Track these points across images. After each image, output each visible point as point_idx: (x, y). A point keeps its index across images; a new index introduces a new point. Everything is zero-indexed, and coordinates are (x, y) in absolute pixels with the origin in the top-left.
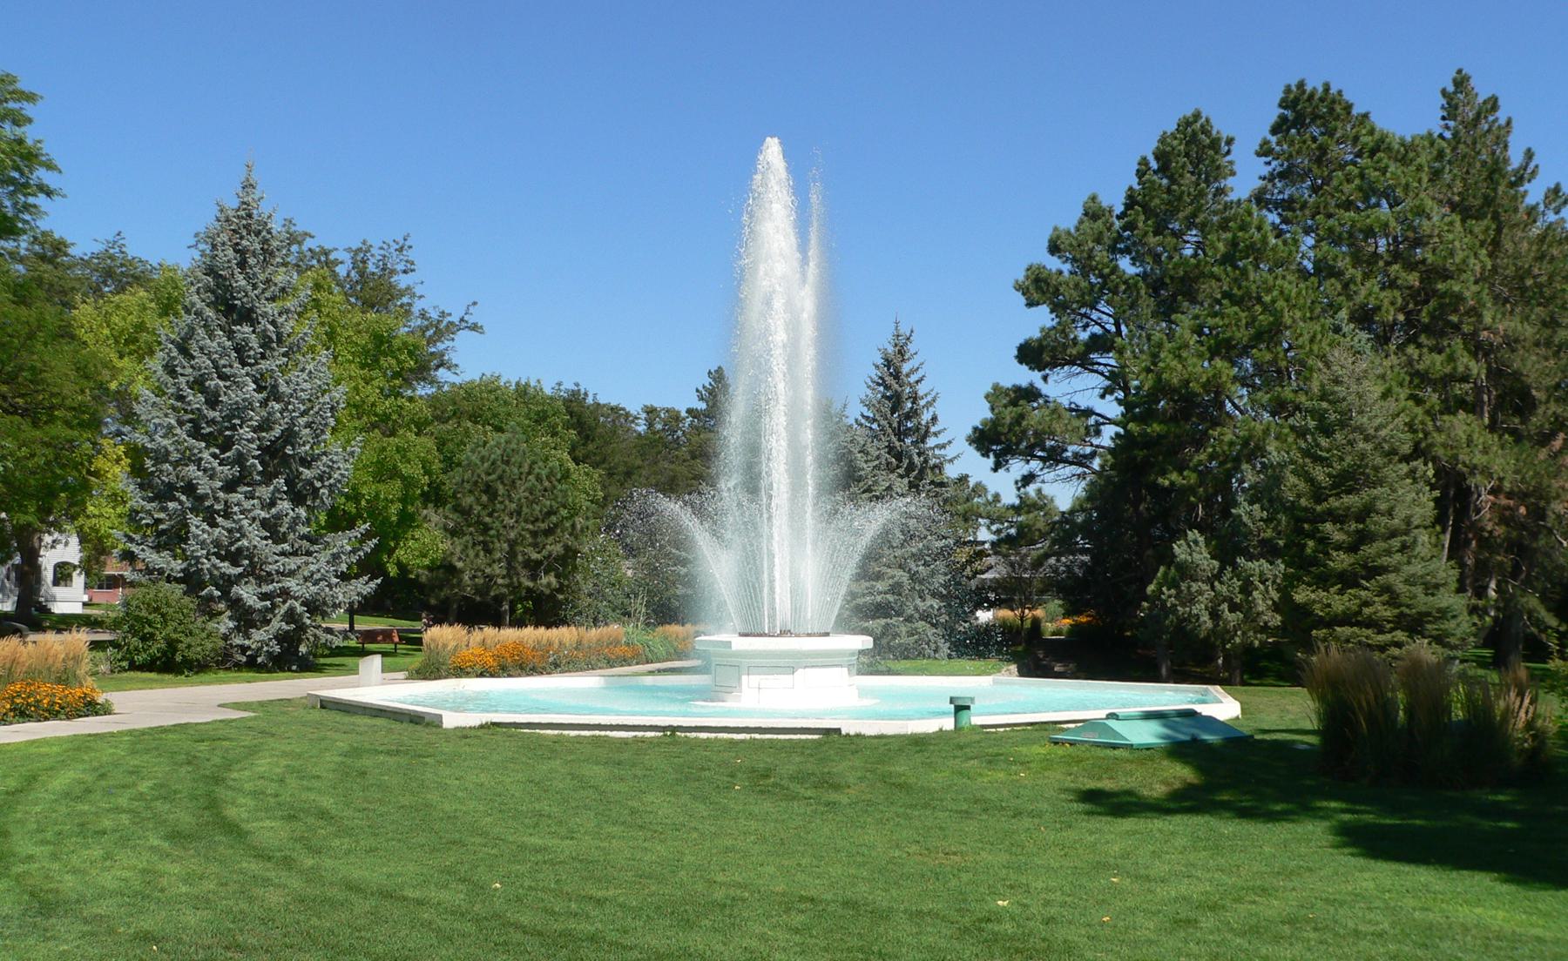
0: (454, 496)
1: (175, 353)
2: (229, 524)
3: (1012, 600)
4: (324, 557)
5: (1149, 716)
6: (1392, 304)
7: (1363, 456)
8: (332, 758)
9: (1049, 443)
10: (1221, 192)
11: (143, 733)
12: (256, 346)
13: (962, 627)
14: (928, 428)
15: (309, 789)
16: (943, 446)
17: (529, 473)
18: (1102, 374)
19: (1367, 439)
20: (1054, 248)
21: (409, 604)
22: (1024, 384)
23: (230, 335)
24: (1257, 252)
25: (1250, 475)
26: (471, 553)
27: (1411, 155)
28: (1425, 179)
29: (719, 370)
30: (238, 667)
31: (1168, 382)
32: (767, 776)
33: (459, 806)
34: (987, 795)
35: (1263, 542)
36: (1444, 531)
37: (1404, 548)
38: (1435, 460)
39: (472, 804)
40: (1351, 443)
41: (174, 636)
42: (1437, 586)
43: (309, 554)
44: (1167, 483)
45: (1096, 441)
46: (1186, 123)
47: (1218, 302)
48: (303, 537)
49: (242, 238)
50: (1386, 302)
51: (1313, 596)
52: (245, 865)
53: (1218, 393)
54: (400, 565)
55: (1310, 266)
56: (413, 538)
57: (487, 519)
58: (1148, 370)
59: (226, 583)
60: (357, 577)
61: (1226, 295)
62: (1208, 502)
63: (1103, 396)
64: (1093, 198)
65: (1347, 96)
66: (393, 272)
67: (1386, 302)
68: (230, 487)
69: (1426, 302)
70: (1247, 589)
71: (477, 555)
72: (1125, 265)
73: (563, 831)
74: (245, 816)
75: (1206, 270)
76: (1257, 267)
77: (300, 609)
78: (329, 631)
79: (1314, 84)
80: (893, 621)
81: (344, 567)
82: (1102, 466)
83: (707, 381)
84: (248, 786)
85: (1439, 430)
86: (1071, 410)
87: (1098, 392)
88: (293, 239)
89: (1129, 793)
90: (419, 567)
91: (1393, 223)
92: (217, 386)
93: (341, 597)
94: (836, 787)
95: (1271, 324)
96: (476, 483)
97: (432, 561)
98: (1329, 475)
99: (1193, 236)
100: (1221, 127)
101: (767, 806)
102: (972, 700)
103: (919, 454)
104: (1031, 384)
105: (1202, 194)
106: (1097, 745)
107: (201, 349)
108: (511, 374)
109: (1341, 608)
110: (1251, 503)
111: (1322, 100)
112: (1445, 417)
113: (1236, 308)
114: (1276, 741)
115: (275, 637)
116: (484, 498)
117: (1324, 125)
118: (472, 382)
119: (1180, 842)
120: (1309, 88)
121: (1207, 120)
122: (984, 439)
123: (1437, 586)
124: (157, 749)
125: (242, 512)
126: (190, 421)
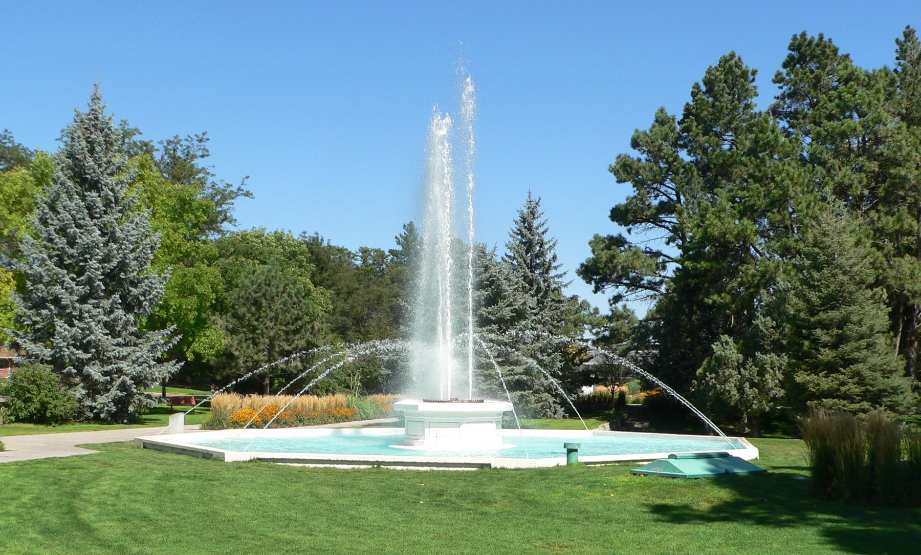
1: (47, 210)
2: (82, 325)
3: (606, 379)
5: (699, 456)
6: (860, 182)
7: (842, 285)
8: (151, 481)
9: (632, 275)
11: (25, 463)
15: (135, 501)
16: (560, 276)
17: (283, 292)
18: (667, 228)
19: (844, 273)
20: (635, 144)
21: (199, 377)
22: (615, 235)
23: (83, 198)
24: (771, 147)
25: (765, 297)
26: (244, 345)
27: (872, 83)
28: (882, 98)
30: (88, 420)
34: (589, 508)
35: (773, 342)
36: (896, 336)
37: (868, 346)
38: (889, 288)
39: (244, 512)
40: (834, 276)
41: (45, 399)
42: (891, 372)
43: (136, 345)
44: (711, 301)
45: (663, 274)
46: (725, 61)
48: (132, 334)
49: (91, 133)
50: (856, 182)
52: (93, 551)
53: (745, 242)
54: (194, 353)
56: (205, 335)
57: (255, 323)
59: (80, 365)
60: (167, 360)
62: (738, 314)
63: (668, 243)
64: (662, 110)
65: (835, 43)
66: (194, 156)
67: (856, 182)
68: (83, 300)
69: (884, 182)
70: (762, 372)
71: (248, 347)
72: (684, 155)
73: (305, 530)
74: (93, 518)
78: (149, 397)
79: (812, 34)
80: (526, 393)
81: (159, 354)
82: (667, 290)
83: (403, 231)
84: (95, 499)
85: (891, 267)
86: (646, 252)
87: (665, 240)
88: (127, 134)
90: (209, 355)
91: (860, 128)
92: (75, 232)
93: (157, 374)
94: (487, 503)
96: (247, 299)
97: (218, 352)
98: (819, 297)
100: (748, 64)
101: (441, 514)
102: (579, 445)
103: (544, 281)
104: (620, 235)
105: (735, 108)
106: (663, 476)
107: (64, 207)
109: (826, 386)
111: (817, 45)
112: (896, 259)
113: (757, 185)
114: (782, 474)
115: (113, 401)
116: (253, 309)
117: (818, 62)
119: (717, 540)
120: (809, 37)
121: (739, 59)
122: (588, 272)
123: (891, 372)
124: (34, 474)
125: (90, 317)
126: (57, 256)
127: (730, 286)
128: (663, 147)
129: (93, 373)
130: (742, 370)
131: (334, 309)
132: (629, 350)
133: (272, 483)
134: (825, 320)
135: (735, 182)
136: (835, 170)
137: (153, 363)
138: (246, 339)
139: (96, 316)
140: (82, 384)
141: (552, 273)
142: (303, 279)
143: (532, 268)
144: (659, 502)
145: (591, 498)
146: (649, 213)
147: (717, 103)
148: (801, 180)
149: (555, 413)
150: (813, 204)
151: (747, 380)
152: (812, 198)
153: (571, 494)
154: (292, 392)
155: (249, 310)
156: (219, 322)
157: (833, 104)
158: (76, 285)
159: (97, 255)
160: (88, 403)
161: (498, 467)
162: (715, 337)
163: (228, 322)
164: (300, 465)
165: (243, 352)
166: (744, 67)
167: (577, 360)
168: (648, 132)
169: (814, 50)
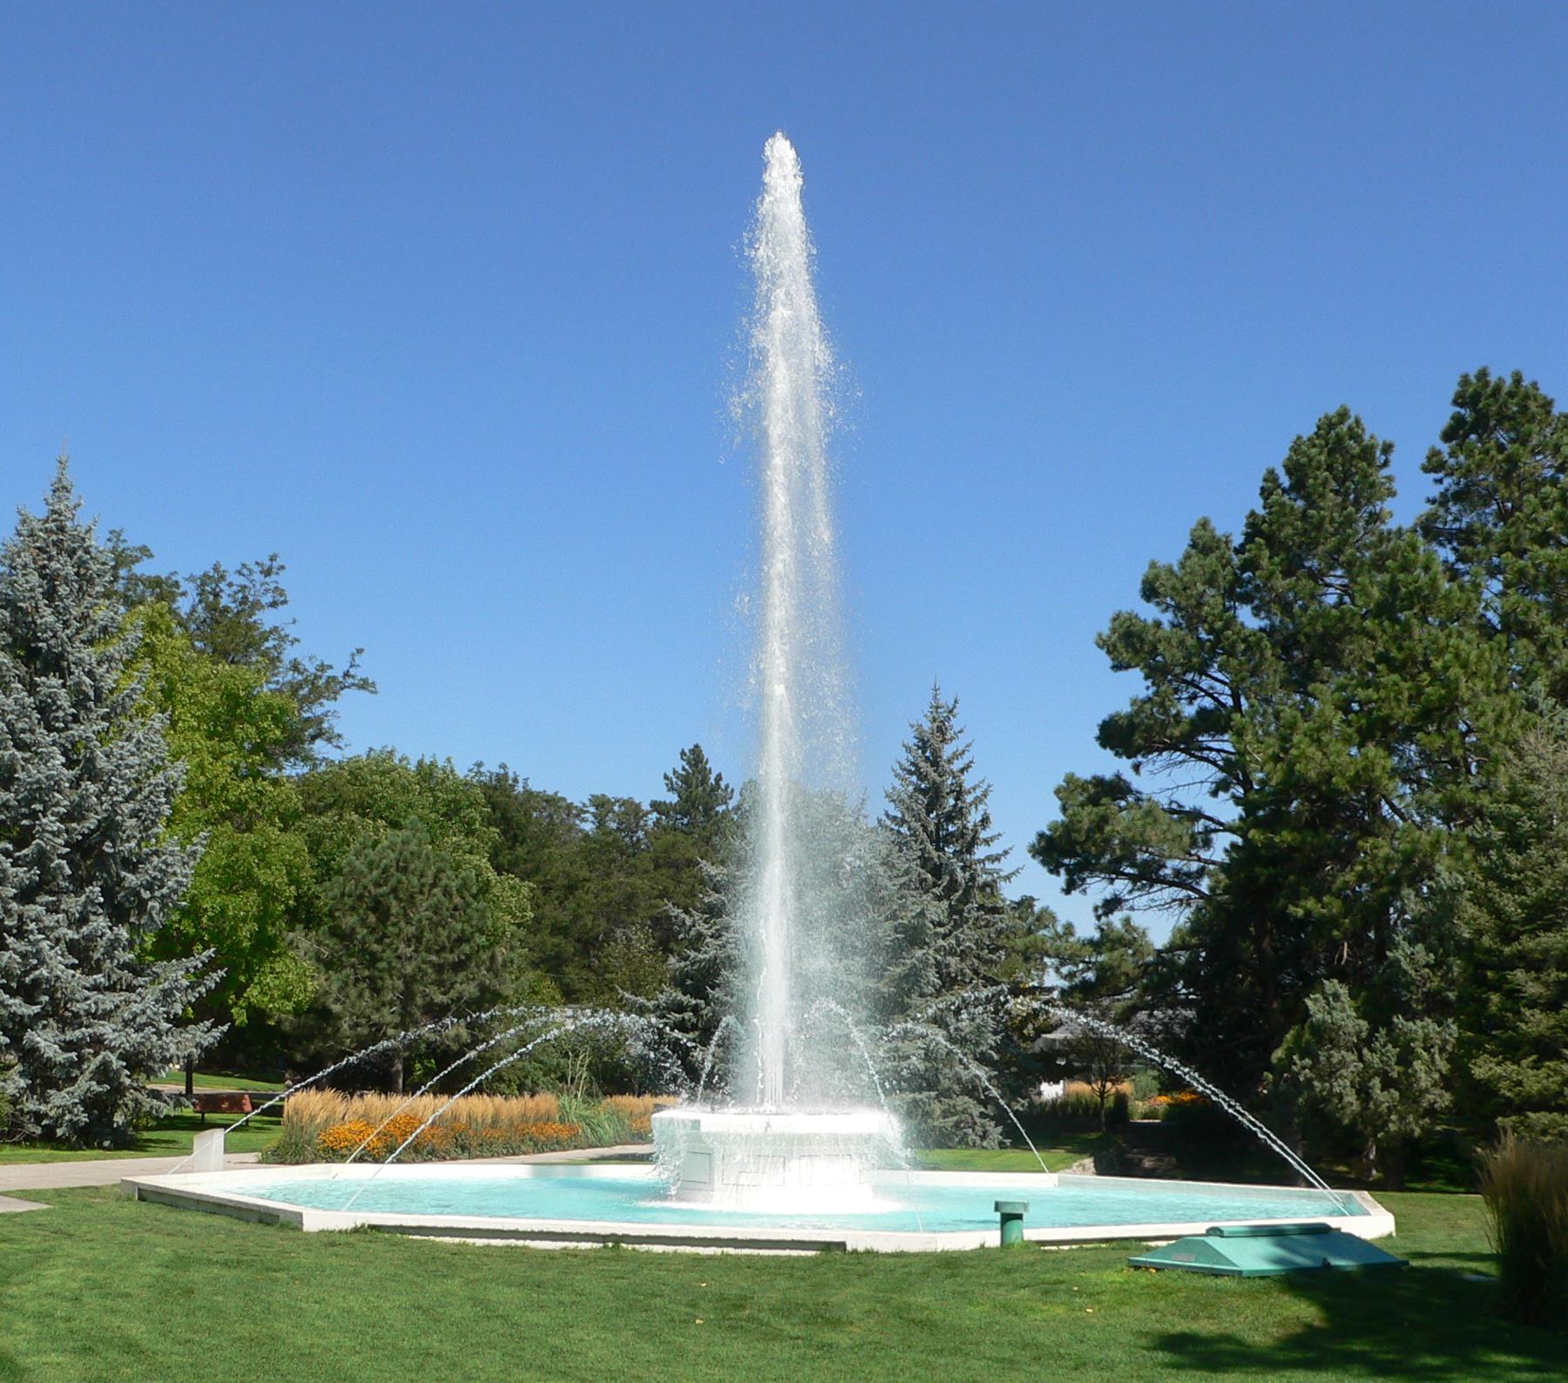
0: (331, 915)
2: (22, 946)
5: (1257, 1232)
8: (148, 1270)
9: (1141, 857)
10: (1375, 518)
12: (66, 705)
13: (1021, 1105)
15: (113, 1312)
16: (997, 858)
17: (434, 885)
18: (1214, 763)
20: (1150, 591)
21: (264, 1058)
22: (1108, 775)
23: (32, 689)
24: (1423, 600)
25: (1412, 903)
26: (353, 992)
29: (696, 750)
30: (31, 1141)
32: (742, 1307)
34: (1041, 1338)
39: (334, 1338)
40: (1551, 861)
43: (131, 988)
44: (1301, 912)
45: (1205, 855)
46: (1328, 426)
47: (1372, 668)
48: (122, 967)
49: (50, 559)
51: (1499, 1070)
53: (1370, 792)
57: (375, 947)
58: (1276, 759)
61: (1383, 658)
62: (1357, 939)
63: (1214, 794)
64: (1204, 524)
65: (1546, 390)
66: (257, 605)
70: (1406, 1058)
71: (360, 996)
72: (1247, 618)
74: (23, 1346)
75: (1355, 626)
77: (117, 1065)
78: (156, 1095)
79: (1501, 373)
81: (178, 1008)
82: (1212, 889)
83: (680, 765)
84: (31, 1306)
87: (1208, 787)
89: (1227, 1338)
90: (281, 1012)
92: (13, 756)
94: (835, 1324)
95: (1442, 698)
96: (360, 898)
98: (1522, 905)
99: (1337, 577)
100: (1375, 430)
101: (738, 1347)
102: (1025, 1206)
103: (964, 869)
104: (1118, 776)
105: (1349, 521)
108: (412, 749)
109: (1536, 1087)
110: (1412, 942)
111: (1511, 395)
113: (1395, 677)
115: (82, 1102)
116: (372, 918)
117: (1514, 429)
118: (357, 759)
120: (1493, 379)
121: (1357, 421)
122: (1054, 850)
125: (40, 931)
128: (1206, 599)
129: (43, 1044)
130: (1365, 1051)
131: (537, 920)
132: (1133, 1009)
133: (394, 1277)
134: (1532, 951)
135: (1348, 670)
136: (1555, 647)
138: (357, 980)
139: (52, 929)
140: (19, 1067)
141: (980, 852)
142: (475, 859)
143: (940, 841)
145: (1047, 1318)
146: (1176, 733)
147: (1312, 512)
149: (984, 1137)
150: (1508, 716)
151: (1377, 1074)
152: (1506, 704)
153: (1005, 1307)
154: (448, 1087)
155: (363, 921)
156: (303, 941)
157: (1551, 513)
158: (13, 865)
159: (57, 804)
160: (31, 1105)
161: (861, 1249)
162: (1311, 984)
163: (319, 943)
164: (457, 1240)
165: (352, 1010)
166: (1366, 437)
167: (1029, 1030)
168: (1176, 568)
169: (1505, 404)
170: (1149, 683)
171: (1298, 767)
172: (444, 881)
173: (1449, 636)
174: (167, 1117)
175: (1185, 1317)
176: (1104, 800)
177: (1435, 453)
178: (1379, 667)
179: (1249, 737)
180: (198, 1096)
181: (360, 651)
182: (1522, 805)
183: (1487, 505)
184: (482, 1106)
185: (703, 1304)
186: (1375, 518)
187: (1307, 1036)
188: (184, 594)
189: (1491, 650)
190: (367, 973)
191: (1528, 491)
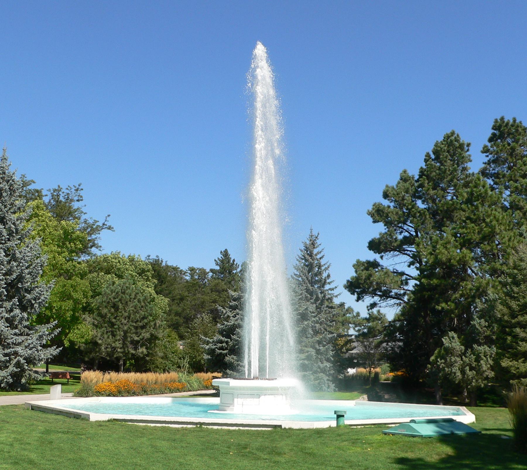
0: (98, 309)
4: (35, 337)
5: (430, 422)
8: (36, 435)
9: (384, 288)
12: (5, 235)
14: (325, 280)
15: (25, 449)
17: (135, 299)
18: (409, 255)
20: (386, 195)
22: (371, 259)
24: (482, 198)
25: (480, 305)
26: (106, 336)
31: (441, 260)
32: (246, 448)
33: (97, 460)
35: (486, 337)
39: (103, 459)
43: (28, 335)
44: (440, 308)
47: (465, 222)
51: (511, 363)
53: (464, 265)
54: (71, 341)
55: (507, 204)
56: (77, 328)
57: (114, 320)
58: (431, 254)
60: (50, 346)
61: (468, 218)
62: (460, 317)
63: (409, 266)
64: (405, 172)
66: (72, 200)
70: (478, 359)
71: (108, 337)
72: (420, 205)
76: (483, 205)
77: (23, 361)
79: (509, 118)
81: (44, 342)
82: (409, 300)
83: (220, 256)
86: (394, 272)
87: (407, 264)
88: (25, 184)
93: (42, 356)
94: (279, 454)
95: (490, 232)
96: (108, 303)
97: (86, 340)
98: (518, 305)
99: (451, 190)
100: (464, 139)
101: (245, 463)
102: (345, 412)
103: (321, 293)
104: (375, 260)
105: (455, 170)
108: (125, 252)
111: (512, 126)
113: (473, 225)
115: (10, 375)
116: (113, 310)
117: (514, 138)
120: (506, 120)
121: (458, 135)
122: (352, 286)
127: (454, 297)
130: (463, 357)
133: (123, 438)
134: (522, 321)
135: (456, 223)
137: (40, 348)
138: (107, 332)
141: (327, 287)
143: (312, 283)
144: (402, 455)
146: (395, 245)
147: (442, 167)
148: (504, 221)
150: (513, 238)
151: (467, 365)
153: (339, 448)
156: (88, 318)
159: (2, 270)
161: (287, 427)
162: (444, 333)
164: (144, 424)
168: (395, 187)
169: (510, 129)
170: (386, 227)
171: (439, 256)
172: (138, 297)
173: (492, 210)
174: (40, 380)
175: (403, 451)
176: (370, 269)
177: (486, 146)
178: (467, 221)
179: (421, 246)
180: (51, 373)
181: (109, 216)
182: (518, 270)
183: (504, 164)
184: (150, 376)
185: (232, 447)
186: (464, 169)
187: (443, 352)
188: (46, 195)
189: (507, 215)
190: (110, 329)
191: (519, 159)
